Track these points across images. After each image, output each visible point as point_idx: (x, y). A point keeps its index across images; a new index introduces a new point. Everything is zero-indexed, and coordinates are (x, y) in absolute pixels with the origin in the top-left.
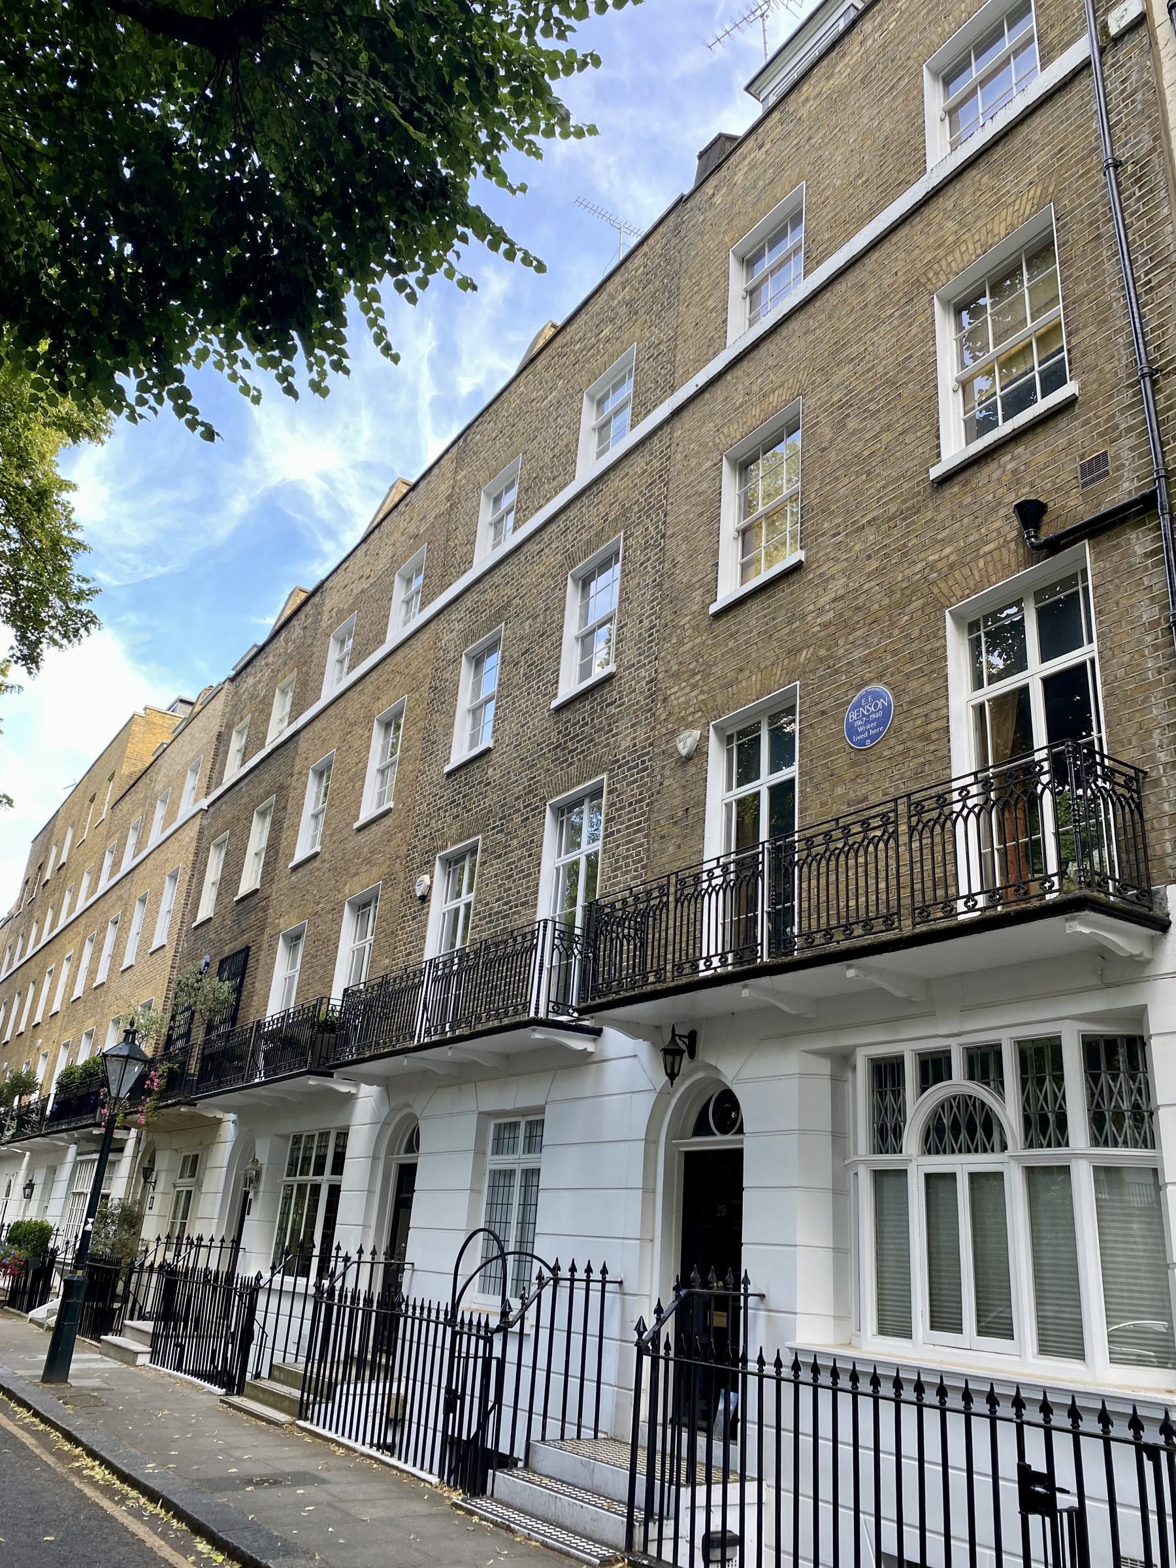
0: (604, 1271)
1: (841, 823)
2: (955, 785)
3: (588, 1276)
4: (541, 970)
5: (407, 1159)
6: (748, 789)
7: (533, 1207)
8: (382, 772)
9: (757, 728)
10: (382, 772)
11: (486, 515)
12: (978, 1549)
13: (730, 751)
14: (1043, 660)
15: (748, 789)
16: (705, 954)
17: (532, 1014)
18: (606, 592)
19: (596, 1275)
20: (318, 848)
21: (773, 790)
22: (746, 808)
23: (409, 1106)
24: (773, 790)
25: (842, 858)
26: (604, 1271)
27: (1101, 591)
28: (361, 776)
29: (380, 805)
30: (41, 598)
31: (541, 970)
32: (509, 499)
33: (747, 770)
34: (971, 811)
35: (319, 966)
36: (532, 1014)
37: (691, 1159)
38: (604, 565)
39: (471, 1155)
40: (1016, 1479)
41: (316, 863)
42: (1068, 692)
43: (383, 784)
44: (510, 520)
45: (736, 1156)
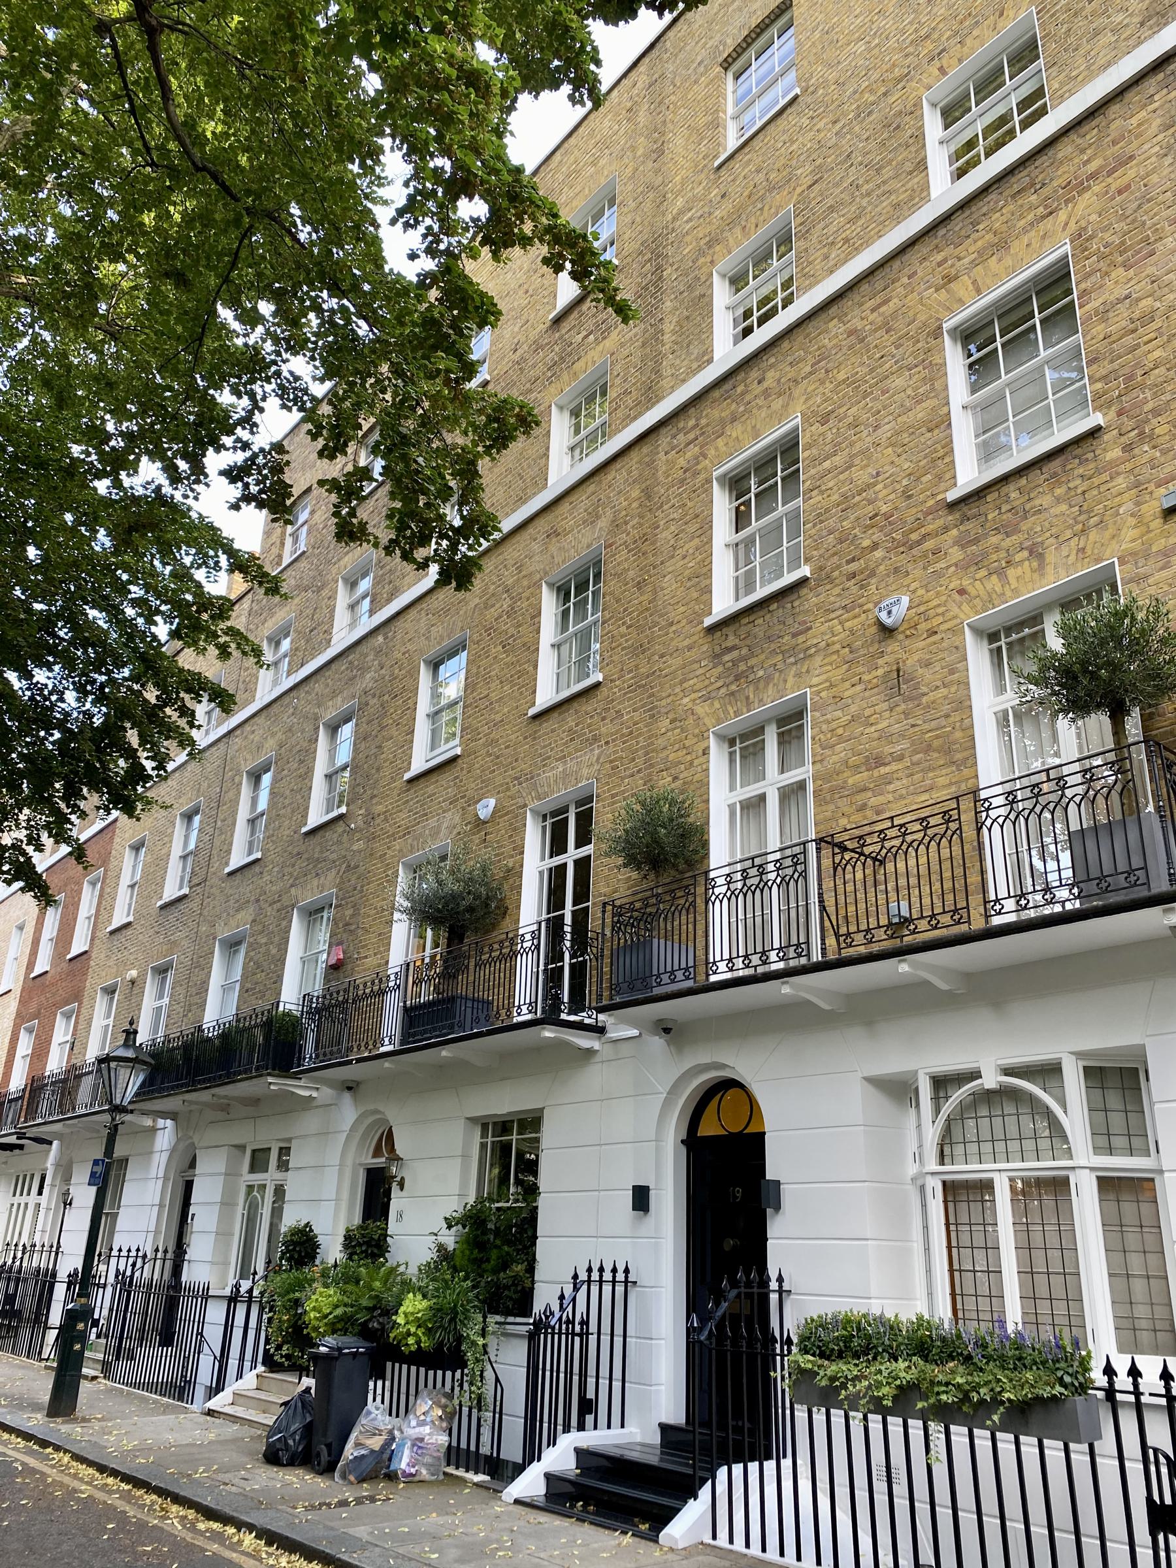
0: (627, 1271)
1: (757, 861)
2: (771, 858)
6: (558, 860)
7: (1072, 1253)
8: (557, 646)
9: (565, 810)
10: (557, 646)
11: (342, 599)
12: (1138, 1549)
13: (544, 828)
15: (558, 860)
16: (669, 969)
18: (454, 680)
19: (620, 1276)
20: (131, 919)
21: (577, 863)
23: (377, 1112)
24: (576, 862)
25: (758, 892)
26: (627, 1271)
28: (533, 649)
29: (250, 853)
32: (365, 585)
33: (558, 845)
34: (910, 845)
35: (266, 971)
38: (452, 653)
39: (459, 1160)
41: (129, 932)
43: (253, 833)
44: (366, 604)
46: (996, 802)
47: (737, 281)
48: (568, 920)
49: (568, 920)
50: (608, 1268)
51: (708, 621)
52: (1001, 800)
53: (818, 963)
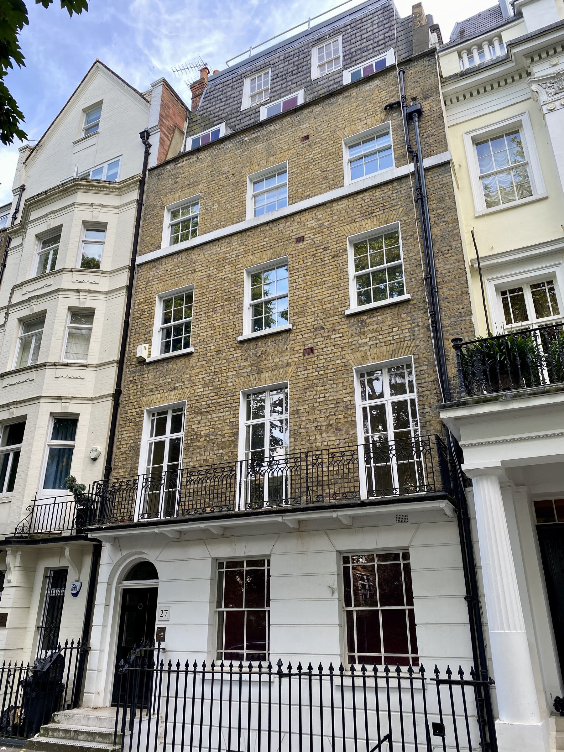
3: (331, 673)
4: (240, 488)
5: (56, 592)
6: (160, 438)
13: (153, 421)
14: (171, 433)
15: (160, 438)
17: (237, 509)
22: (160, 446)
27: (421, 411)
30: (37, 2)
31: (240, 488)
33: (160, 431)
34: (280, 469)
36: (237, 509)
37: (126, 592)
39: (336, 576)
40: (426, 743)
42: (175, 445)
45: (154, 592)
46: (281, 462)
47: (174, 214)
48: (165, 469)
49: (165, 469)
50: (70, 642)
51: (240, 338)
52: (283, 462)
53: (136, 523)
